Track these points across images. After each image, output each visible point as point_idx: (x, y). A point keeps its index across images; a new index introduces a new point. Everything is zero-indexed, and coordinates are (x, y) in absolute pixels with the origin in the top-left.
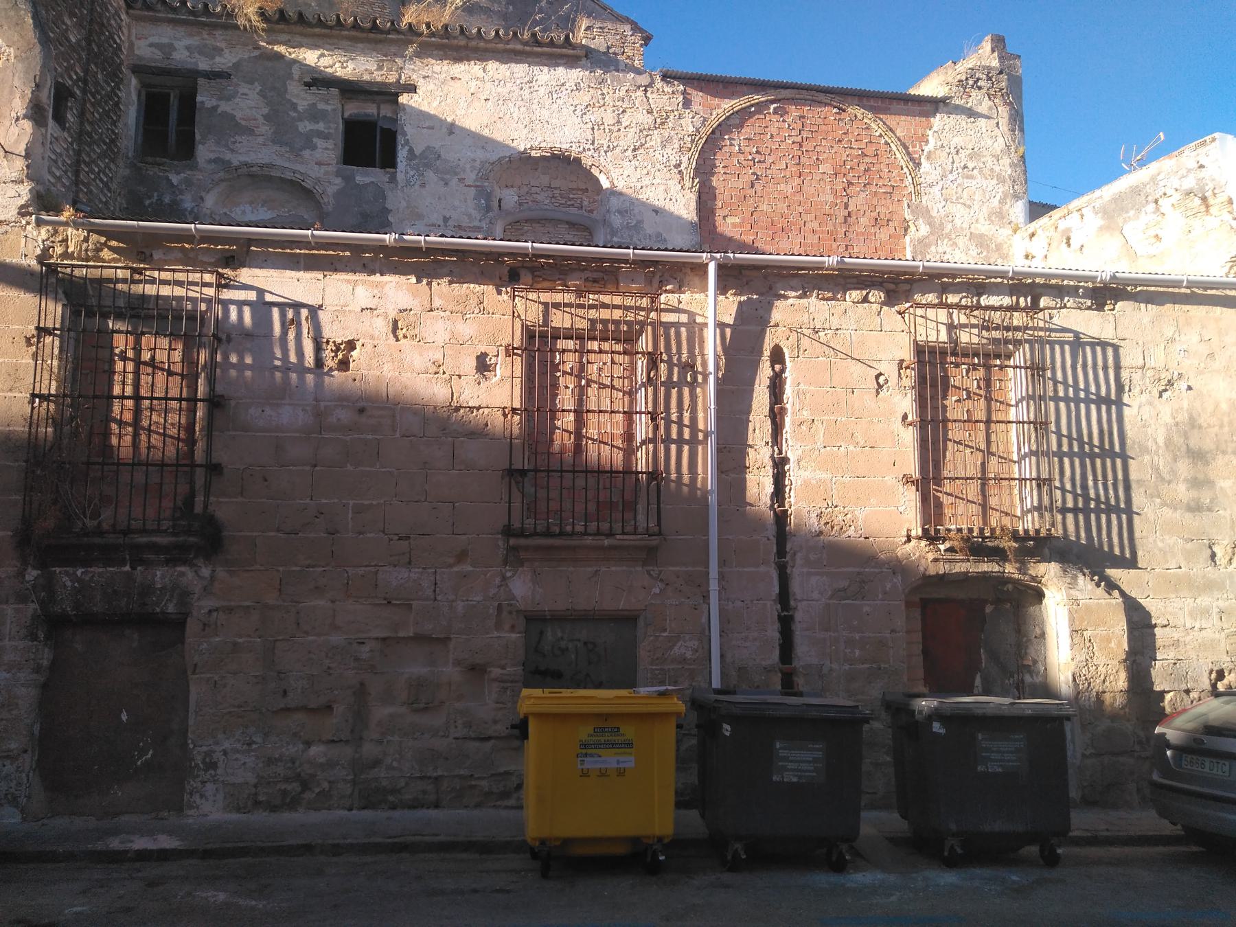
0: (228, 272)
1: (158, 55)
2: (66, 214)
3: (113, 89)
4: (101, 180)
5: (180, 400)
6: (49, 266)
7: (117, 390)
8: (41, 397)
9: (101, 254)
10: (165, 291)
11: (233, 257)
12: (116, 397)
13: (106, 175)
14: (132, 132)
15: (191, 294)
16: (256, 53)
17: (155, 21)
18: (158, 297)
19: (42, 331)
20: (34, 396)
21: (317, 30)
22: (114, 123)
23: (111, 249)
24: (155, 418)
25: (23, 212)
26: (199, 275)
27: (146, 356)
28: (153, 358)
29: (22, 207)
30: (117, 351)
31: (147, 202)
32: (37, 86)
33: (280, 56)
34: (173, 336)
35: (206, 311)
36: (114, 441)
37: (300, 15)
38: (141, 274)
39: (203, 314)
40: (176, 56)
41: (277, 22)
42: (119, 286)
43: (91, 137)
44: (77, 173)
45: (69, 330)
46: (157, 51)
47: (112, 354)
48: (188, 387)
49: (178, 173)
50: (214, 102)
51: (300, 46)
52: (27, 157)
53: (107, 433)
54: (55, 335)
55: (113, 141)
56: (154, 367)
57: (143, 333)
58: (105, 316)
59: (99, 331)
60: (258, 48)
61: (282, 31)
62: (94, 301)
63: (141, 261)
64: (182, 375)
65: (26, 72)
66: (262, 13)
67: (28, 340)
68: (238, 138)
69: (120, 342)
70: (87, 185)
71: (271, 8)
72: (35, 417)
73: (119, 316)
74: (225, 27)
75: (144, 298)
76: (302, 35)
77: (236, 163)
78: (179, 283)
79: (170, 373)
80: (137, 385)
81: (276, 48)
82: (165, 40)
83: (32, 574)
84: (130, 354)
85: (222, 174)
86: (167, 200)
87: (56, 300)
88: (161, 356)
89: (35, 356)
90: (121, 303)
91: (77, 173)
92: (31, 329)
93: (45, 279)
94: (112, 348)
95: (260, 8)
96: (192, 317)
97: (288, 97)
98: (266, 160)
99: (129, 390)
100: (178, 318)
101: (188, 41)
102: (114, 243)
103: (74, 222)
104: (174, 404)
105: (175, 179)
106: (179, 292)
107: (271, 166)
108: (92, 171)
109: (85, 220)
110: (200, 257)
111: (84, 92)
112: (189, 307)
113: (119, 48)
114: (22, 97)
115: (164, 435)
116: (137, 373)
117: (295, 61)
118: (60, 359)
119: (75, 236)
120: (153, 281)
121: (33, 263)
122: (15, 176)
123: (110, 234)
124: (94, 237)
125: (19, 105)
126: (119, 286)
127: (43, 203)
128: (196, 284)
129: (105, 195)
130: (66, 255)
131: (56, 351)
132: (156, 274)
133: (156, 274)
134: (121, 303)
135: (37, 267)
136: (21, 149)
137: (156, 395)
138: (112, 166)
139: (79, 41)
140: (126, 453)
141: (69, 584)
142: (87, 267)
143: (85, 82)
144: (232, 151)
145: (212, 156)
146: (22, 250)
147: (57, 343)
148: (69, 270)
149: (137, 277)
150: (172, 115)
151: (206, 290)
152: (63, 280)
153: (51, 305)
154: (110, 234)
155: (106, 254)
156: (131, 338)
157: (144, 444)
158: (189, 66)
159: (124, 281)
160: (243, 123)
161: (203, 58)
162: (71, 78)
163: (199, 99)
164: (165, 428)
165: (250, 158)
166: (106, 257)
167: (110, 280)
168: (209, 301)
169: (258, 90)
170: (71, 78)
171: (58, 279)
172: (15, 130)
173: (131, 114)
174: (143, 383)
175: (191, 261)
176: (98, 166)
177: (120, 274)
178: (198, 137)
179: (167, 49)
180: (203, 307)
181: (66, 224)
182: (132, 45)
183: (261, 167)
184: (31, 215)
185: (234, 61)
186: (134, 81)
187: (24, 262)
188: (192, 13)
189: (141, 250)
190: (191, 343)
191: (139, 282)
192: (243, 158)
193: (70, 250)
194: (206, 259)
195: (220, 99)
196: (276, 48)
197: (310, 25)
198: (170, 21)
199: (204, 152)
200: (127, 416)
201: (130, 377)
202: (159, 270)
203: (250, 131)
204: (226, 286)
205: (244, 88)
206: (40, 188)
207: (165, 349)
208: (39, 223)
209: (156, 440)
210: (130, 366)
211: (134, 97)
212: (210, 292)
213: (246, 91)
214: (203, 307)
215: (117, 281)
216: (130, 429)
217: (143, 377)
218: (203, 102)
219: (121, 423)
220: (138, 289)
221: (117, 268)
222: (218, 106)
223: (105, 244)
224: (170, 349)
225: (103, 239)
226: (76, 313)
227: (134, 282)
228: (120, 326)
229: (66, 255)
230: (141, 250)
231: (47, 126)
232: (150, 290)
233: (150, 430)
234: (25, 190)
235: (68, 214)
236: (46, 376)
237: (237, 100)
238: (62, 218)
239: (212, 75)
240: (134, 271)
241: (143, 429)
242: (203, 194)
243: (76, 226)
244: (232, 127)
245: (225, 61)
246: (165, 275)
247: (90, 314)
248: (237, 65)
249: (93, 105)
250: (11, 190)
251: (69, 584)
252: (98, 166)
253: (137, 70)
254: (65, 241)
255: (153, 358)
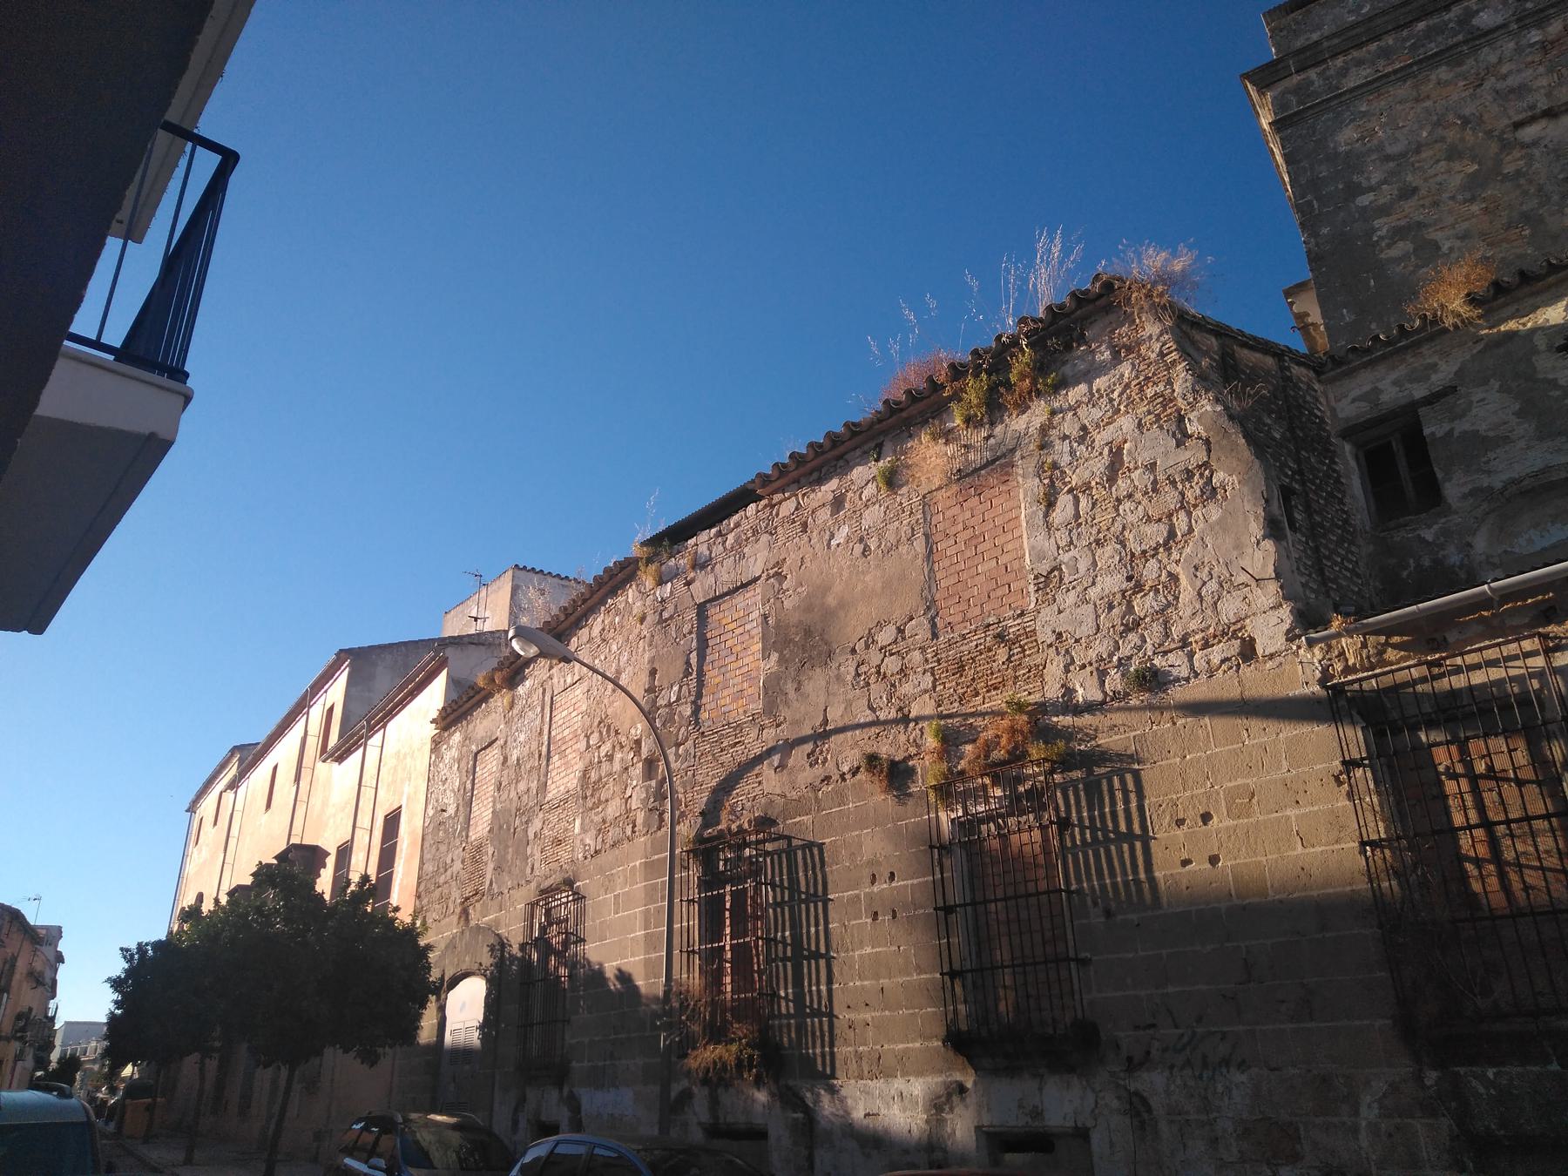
0: (1553, 629)
1: (1364, 406)
2: (1336, 624)
3: (1329, 467)
4: (1347, 569)
5: (1547, 817)
6: (1334, 687)
7: (1458, 820)
8: (1373, 844)
9: (1386, 656)
10: (1478, 678)
11: (1553, 608)
12: (1461, 829)
13: (1350, 561)
14: (1362, 502)
15: (1512, 672)
16: (1480, 346)
17: (1350, 373)
18: (1471, 688)
19: (1350, 764)
20: (1363, 844)
21: (1551, 279)
22: (1341, 502)
23: (1395, 646)
24: (1520, 847)
25: (1291, 637)
26: (1515, 645)
27: (1481, 767)
28: (1490, 768)
29: (1288, 632)
30: (1441, 769)
31: (1405, 574)
32: (1267, 501)
33: (1512, 335)
34: (1508, 733)
35: (1541, 689)
36: (1476, 886)
37: (1522, 273)
38: (1440, 665)
39: (1538, 693)
40: (1384, 398)
41: (1495, 298)
42: (1419, 688)
43: (1323, 527)
44: (1321, 572)
45: (1379, 757)
46: (1363, 404)
47: (1438, 774)
48: (1551, 796)
49: (1429, 527)
50: (1446, 427)
51: (1534, 309)
52: (1278, 577)
53: (1464, 877)
54: (1365, 766)
55: (1346, 521)
56: (1497, 779)
57: (1468, 739)
58: (1414, 729)
59: (1414, 749)
60: (1480, 339)
61: (1506, 305)
62: (1395, 715)
63: (1434, 651)
64: (1539, 783)
65: (1253, 492)
66: (1472, 300)
67: (1337, 778)
68: (1491, 455)
69: (1443, 758)
70: (1335, 581)
71: (1481, 287)
72: (1373, 870)
73: (1431, 725)
74: (1431, 338)
75: (1453, 693)
76: (1533, 294)
77: (1498, 485)
78: (1491, 663)
79: (1520, 783)
80: (1481, 808)
81: (1502, 328)
82: (1367, 388)
83: (1431, 1076)
84: (1459, 769)
85: (1485, 506)
86: (1426, 562)
87: (1353, 724)
88: (1501, 762)
89: (1350, 795)
90: (1427, 708)
91: (1321, 572)
92: (1337, 765)
93: (1334, 704)
94: (1435, 767)
95: (1468, 295)
96: (1524, 701)
97: (1541, 376)
98: (1539, 465)
99: (1473, 816)
100: (1506, 707)
101: (1394, 376)
102: (1396, 639)
103: (1347, 630)
104: (1540, 825)
105: (1428, 535)
106: (1496, 674)
107: (1547, 469)
108: (1336, 564)
109: (1357, 624)
110: (1509, 622)
111: (1303, 483)
112: (1516, 690)
113: (1322, 420)
114: (1257, 518)
115: (1542, 868)
116: (1476, 792)
117: (1534, 331)
118: (1379, 794)
119: (1350, 644)
120: (1458, 670)
121: (1317, 688)
122: (1272, 601)
123: (1387, 630)
124: (1372, 639)
125: (1256, 528)
126: (1419, 688)
127: (1308, 621)
128: (1516, 657)
129: (1356, 584)
130: (1348, 670)
131: (1372, 786)
132: (1459, 661)
133: (1459, 661)
134: (1427, 708)
135: (1323, 693)
136: (1270, 572)
137: (1511, 816)
138: (1353, 549)
139: (1283, 435)
140: (1498, 900)
141: (1482, 1090)
142: (1376, 676)
143: (1300, 472)
144: (1489, 472)
145: (1466, 490)
146: (1302, 678)
147: (1369, 775)
148: (1356, 686)
149: (1436, 671)
150: (1401, 460)
151: (1531, 662)
152: (1353, 698)
153: (1349, 731)
154: (1387, 630)
155: (1391, 654)
156: (1453, 748)
157: (1516, 886)
158: (1403, 402)
159: (1423, 680)
160: (1491, 434)
161: (1415, 386)
162: (1286, 475)
163: (1426, 432)
164: (1539, 859)
165: (1518, 471)
166: (1393, 658)
167: (1406, 684)
168: (1540, 675)
169: (1497, 385)
170: (1286, 475)
171: (1349, 700)
172: (1259, 555)
173: (1355, 484)
174: (1487, 802)
175: (1497, 629)
176: (1339, 555)
177: (1415, 673)
178: (1440, 475)
179: (1372, 396)
180: (1536, 684)
181: (1338, 635)
182: (1333, 410)
183: (1535, 475)
184: (1299, 637)
185: (1455, 368)
186: (1348, 447)
187: (1307, 691)
188: (1388, 343)
189: (1431, 636)
190: (1534, 735)
191: (1442, 675)
192: (1505, 477)
193: (1351, 662)
194: (1515, 622)
195: (1452, 420)
196: (1502, 328)
197: (1539, 278)
198: (1365, 366)
199: (1454, 490)
200: (1482, 851)
201: (1468, 798)
202: (1462, 654)
203: (1506, 440)
204: (1558, 648)
205: (1478, 394)
206: (1300, 605)
207: (1505, 754)
208: (1311, 643)
209: (1532, 878)
210: (1464, 784)
211: (1353, 463)
212: (1538, 662)
213: (1480, 396)
214: (1536, 684)
215: (1415, 682)
216: (1492, 867)
217: (1485, 795)
218: (1433, 434)
219: (1478, 862)
220: (1443, 684)
221: (1409, 667)
222: (1452, 430)
223: (1387, 644)
224: (1510, 751)
225: (1383, 639)
226: (1379, 734)
227: (1435, 678)
228: (1437, 736)
229: (1348, 670)
230: (1431, 636)
231: (1286, 537)
232: (1459, 682)
233: (1520, 866)
234: (1285, 612)
235: (1337, 623)
236: (1370, 817)
237: (1474, 411)
238: (1332, 630)
239: (1432, 399)
240: (1430, 664)
241: (1509, 864)
242: (1469, 539)
243: (1349, 633)
244: (1478, 446)
245: (1444, 373)
246: (1471, 659)
247: (1397, 731)
248: (1460, 373)
249: (1315, 492)
250: (1273, 617)
251: (1482, 1090)
252: (1339, 555)
253: (1346, 434)
254: (1342, 654)
255: (1490, 768)
